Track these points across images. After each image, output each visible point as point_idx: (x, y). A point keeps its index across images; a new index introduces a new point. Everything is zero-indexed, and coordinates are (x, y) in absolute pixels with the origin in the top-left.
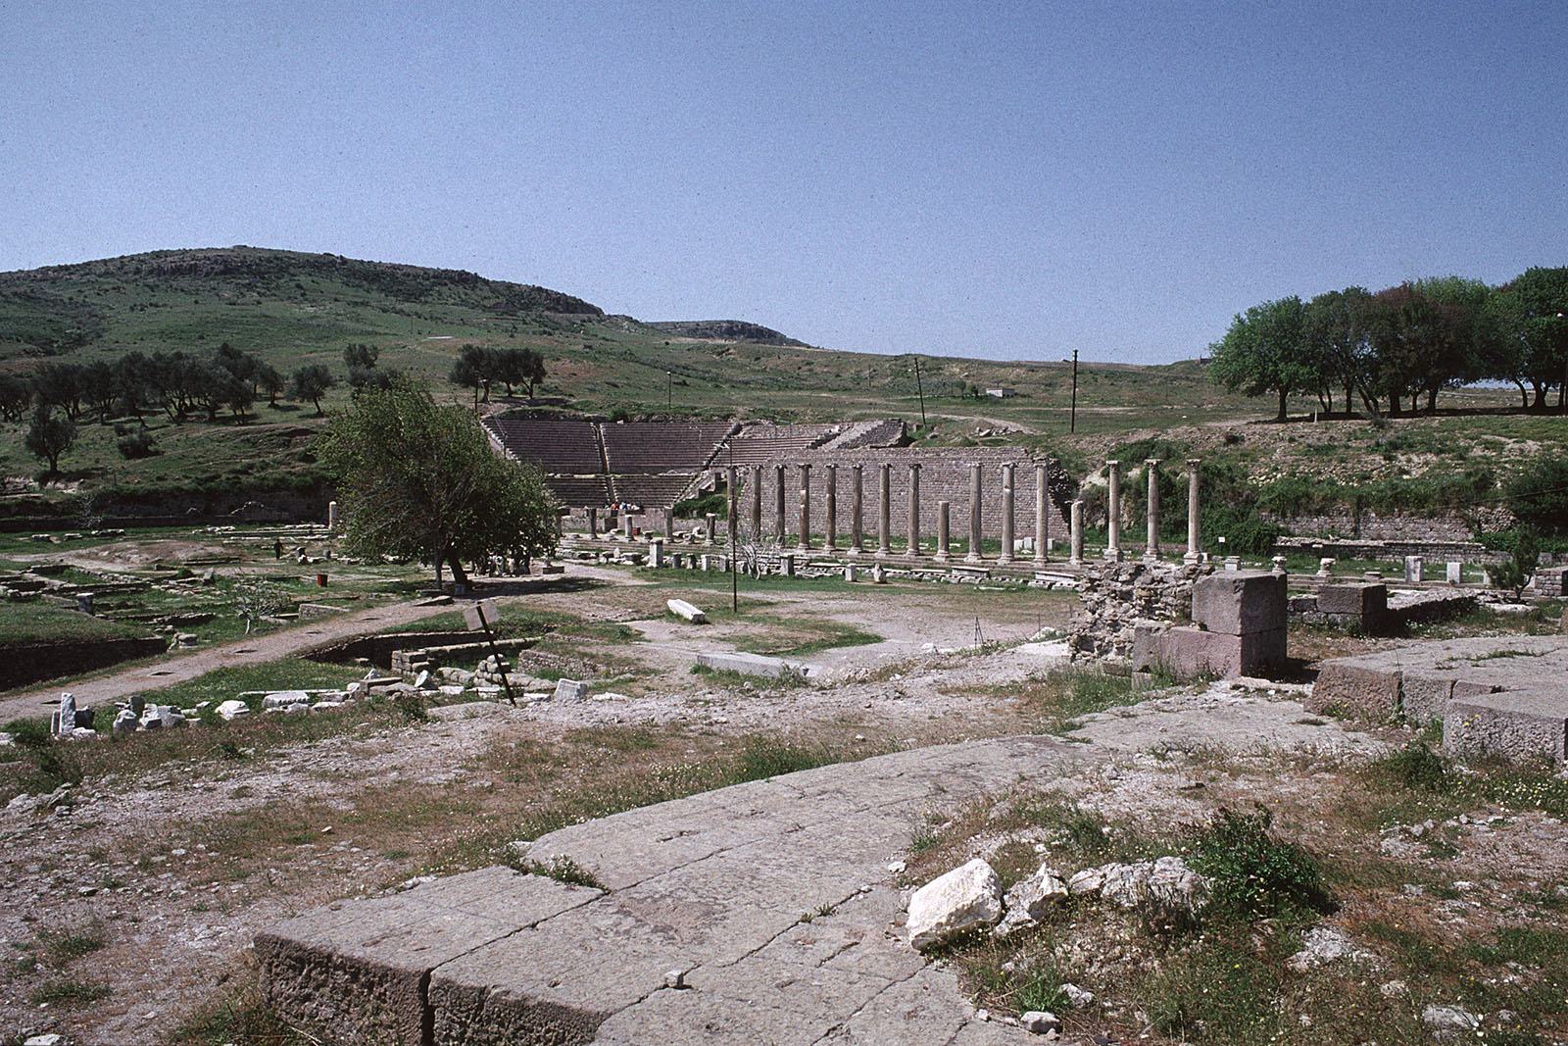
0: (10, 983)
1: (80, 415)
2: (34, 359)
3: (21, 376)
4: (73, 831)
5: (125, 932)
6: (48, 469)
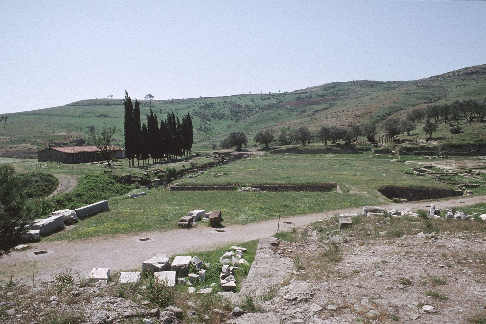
0: (419, 287)
1: (439, 121)
2: (426, 104)
3: (423, 110)
4: (437, 246)
5: (453, 282)
6: (429, 137)
